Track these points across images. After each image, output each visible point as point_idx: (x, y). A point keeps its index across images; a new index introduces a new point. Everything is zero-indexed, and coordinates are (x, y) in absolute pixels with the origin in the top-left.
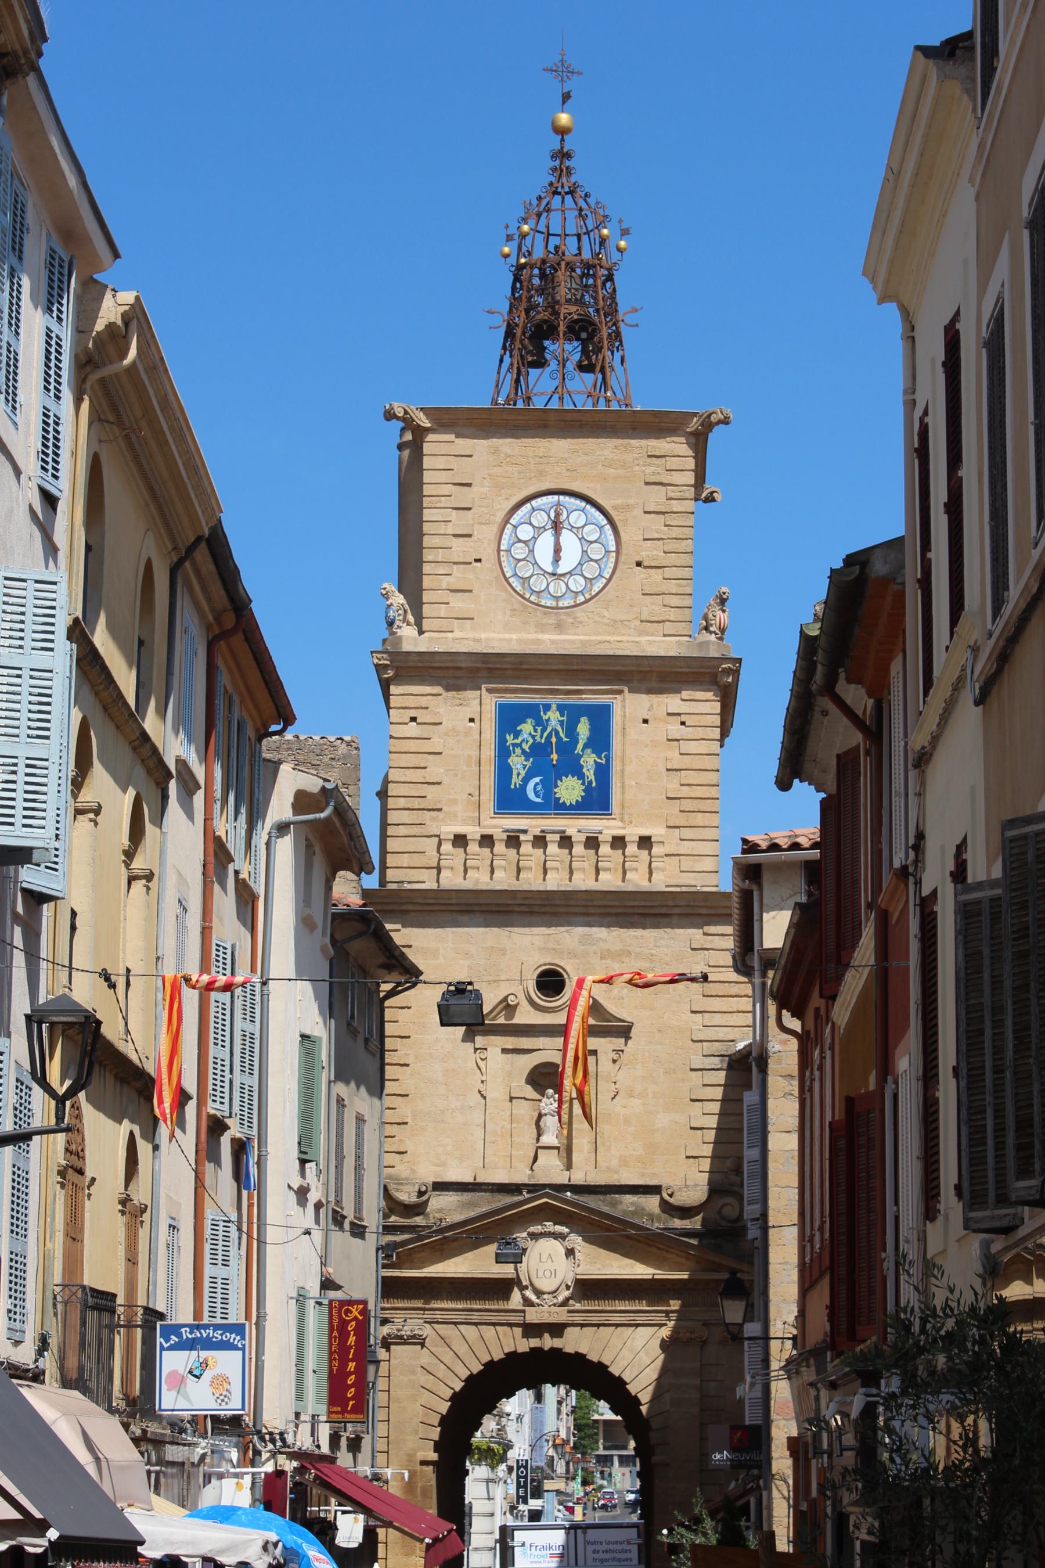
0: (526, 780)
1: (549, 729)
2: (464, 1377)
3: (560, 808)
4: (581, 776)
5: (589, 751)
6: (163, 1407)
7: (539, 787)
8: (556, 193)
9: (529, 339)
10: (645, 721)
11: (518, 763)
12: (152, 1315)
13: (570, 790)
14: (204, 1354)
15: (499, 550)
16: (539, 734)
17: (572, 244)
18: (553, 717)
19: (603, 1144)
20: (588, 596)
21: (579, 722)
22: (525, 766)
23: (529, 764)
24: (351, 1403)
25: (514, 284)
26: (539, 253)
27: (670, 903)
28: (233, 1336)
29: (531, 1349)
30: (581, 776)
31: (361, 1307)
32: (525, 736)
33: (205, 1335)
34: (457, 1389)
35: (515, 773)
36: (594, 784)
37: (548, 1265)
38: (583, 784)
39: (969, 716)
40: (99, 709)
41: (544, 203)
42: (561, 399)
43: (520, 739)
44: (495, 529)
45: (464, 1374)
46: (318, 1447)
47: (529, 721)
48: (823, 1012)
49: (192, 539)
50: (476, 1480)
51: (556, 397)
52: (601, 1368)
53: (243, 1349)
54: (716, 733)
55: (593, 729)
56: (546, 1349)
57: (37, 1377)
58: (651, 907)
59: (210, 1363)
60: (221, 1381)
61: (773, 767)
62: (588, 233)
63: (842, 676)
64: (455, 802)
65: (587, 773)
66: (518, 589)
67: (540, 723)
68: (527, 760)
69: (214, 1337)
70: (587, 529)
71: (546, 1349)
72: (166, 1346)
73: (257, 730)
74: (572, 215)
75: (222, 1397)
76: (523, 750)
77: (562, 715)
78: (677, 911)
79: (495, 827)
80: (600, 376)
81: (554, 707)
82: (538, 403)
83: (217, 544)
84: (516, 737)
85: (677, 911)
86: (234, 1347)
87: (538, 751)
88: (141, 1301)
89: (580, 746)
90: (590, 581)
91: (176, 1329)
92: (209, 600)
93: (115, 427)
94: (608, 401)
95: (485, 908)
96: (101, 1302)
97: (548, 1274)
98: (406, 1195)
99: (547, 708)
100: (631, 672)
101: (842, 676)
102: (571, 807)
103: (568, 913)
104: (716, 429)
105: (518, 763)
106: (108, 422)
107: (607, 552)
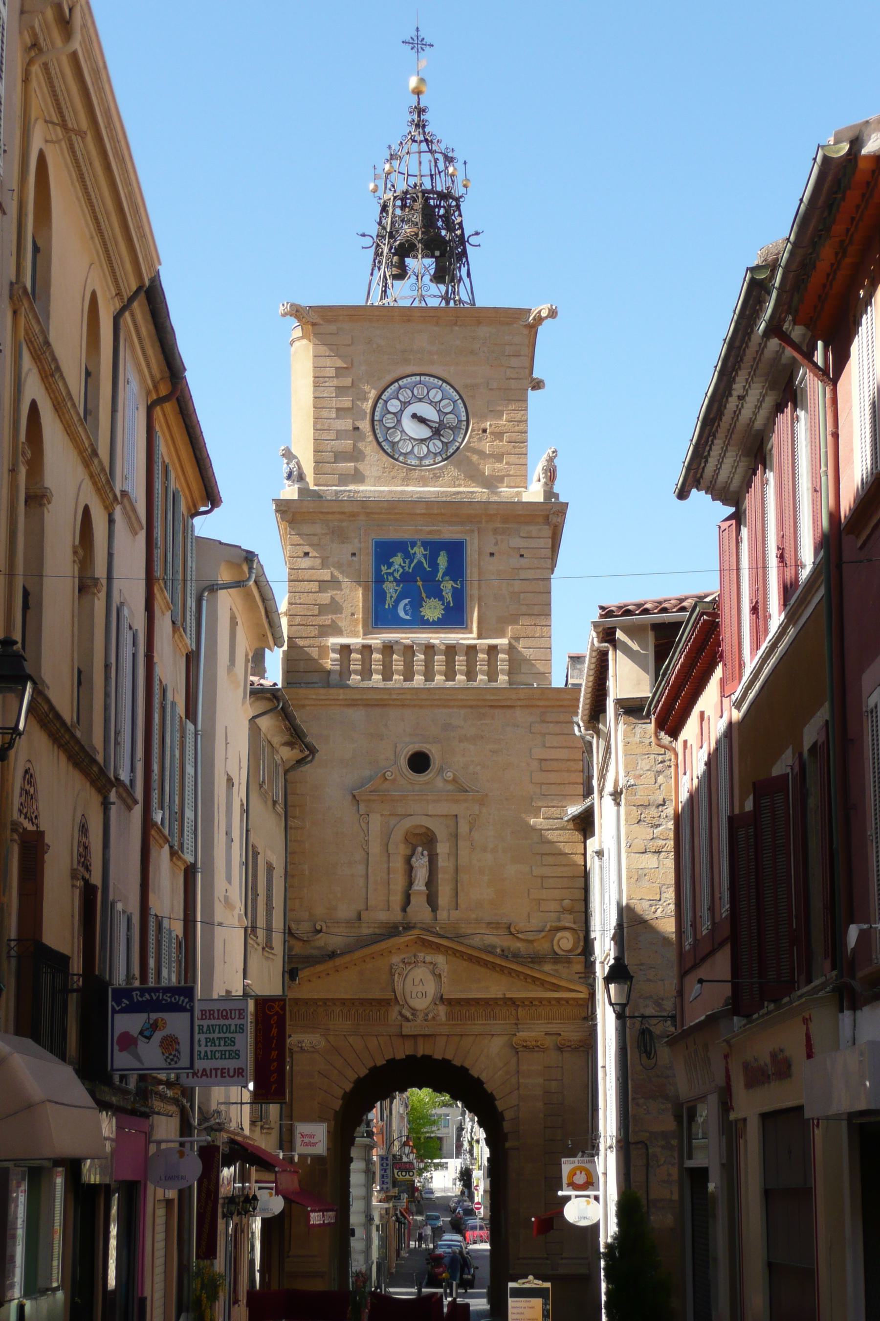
0: (397, 602)
1: (415, 561)
2: (369, 1067)
3: (424, 624)
4: (441, 598)
5: (447, 578)
6: (115, 1067)
7: (408, 608)
10: (492, 554)
11: (391, 589)
14: (154, 1016)
16: (407, 565)
18: (419, 552)
21: (439, 555)
22: (396, 590)
23: (399, 589)
24: (274, 1087)
25: (381, 213)
26: (402, 186)
27: (514, 697)
28: (182, 998)
29: (407, 1056)
30: (441, 598)
31: (282, 1003)
32: (397, 567)
33: (154, 998)
34: (348, 1090)
35: (388, 595)
36: (452, 605)
37: (420, 988)
38: (443, 604)
43: (392, 569)
45: (353, 1077)
46: (242, 1129)
47: (399, 554)
49: (134, 288)
51: (417, 299)
52: (463, 1071)
54: (548, 552)
55: (450, 561)
58: (498, 700)
59: (160, 1024)
60: (169, 1044)
62: (440, 173)
65: (446, 596)
66: (389, 451)
67: (408, 556)
68: (398, 585)
69: (163, 999)
70: (443, 403)
72: (117, 1009)
73: (189, 510)
75: (171, 1057)
76: (395, 578)
77: (425, 550)
78: (519, 703)
81: (419, 543)
83: (152, 298)
84: (389, 568)
85: (519, 703)
87: (406, 578)
89: (440, 574)
93: (58, 128)
97: (420, 995)
99: (413, 544)
102: (434, 623)
103: (431, 706)
104: (545, 323)
105: (391, 589)
107: (460, 421)
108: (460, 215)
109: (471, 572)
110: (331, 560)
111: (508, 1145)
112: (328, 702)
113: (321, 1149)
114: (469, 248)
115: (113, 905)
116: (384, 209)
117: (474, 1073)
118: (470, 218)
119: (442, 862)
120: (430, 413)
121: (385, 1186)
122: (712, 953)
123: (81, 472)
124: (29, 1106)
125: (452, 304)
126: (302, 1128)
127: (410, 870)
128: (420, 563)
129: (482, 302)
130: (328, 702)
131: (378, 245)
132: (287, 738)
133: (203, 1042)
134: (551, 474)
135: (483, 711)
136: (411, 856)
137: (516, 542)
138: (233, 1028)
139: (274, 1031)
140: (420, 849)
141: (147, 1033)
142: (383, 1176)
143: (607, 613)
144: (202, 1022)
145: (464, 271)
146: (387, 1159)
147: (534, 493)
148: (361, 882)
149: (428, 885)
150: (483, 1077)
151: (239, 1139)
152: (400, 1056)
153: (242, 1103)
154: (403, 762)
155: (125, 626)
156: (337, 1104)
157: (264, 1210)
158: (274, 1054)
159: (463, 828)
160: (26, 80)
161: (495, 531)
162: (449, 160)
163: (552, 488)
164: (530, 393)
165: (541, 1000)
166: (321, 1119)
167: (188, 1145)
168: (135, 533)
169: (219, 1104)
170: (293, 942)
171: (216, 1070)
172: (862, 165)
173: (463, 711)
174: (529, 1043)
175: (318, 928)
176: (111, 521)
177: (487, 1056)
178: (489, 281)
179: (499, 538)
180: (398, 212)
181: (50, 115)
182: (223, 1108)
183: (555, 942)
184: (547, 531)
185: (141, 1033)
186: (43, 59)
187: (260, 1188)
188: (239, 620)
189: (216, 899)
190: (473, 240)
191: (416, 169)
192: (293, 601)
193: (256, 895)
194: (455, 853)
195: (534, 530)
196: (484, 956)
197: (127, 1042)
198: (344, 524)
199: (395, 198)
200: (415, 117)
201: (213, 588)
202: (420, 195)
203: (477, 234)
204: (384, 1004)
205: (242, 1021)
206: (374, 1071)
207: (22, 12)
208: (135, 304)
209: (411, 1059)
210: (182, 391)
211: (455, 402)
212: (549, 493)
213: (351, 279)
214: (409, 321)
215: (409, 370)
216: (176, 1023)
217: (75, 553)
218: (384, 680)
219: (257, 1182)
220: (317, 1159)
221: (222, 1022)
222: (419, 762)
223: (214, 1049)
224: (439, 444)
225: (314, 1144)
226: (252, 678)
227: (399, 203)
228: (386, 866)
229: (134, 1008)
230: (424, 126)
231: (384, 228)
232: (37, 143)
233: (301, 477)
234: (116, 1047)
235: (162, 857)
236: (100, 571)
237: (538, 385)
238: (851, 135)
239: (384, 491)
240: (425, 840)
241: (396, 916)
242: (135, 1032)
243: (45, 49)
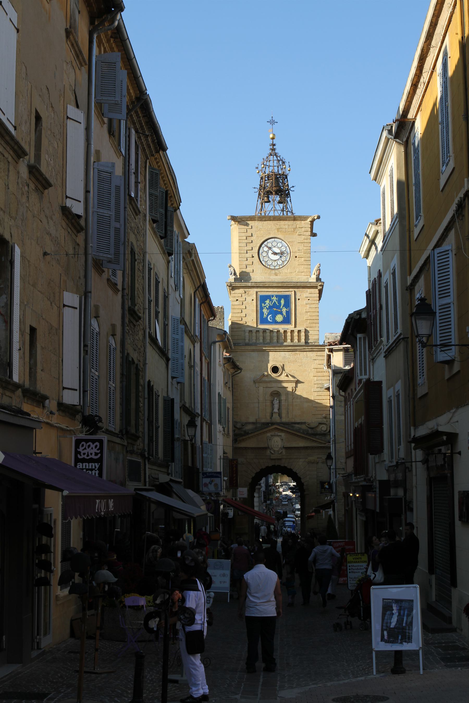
0: (268, 316)
3: (276, 322)
9: (265, 194)
11: (265, 311)
13: (279, 318)
14: (212, 479)
18: (274, 299)
48: (350, 394)
52: (291, 470)
53: (221, 478)
54: (318, 299)
60: (216, 485)
66: (264, 264)
87: (270, 307)
90: (283, 262)
98: (239, 426)
105: (265, 311)
108: (287, 180)
111: (305, 493)
113: (246, 496)
114: (290, 192)
116: (262, 178)
117: (294, 470)
118: (291, 181)
119: (283, 403)
120: (277, 251)
122: (350, 457)
127: (273, 405)
128: (275, 302)
132: (232, 367)
136: (273, 400)
139: (234, 469)
140: (276, 398)
141: (211, 483)
149: (278, 410)
150: (297, 472)
152: (270, 465)
156: (250, 481)
158: (234, 475)
162: (284, 163)
177: (299, 465)
190: (292, 189)
197: (206, 485)
200: (272, 147)
201: (215, 342)
203: (293, 187)
204: (266, 448)
206: (262, 470)
208: (200, 289)
209: (274, 466)
220: (244, 498)
229: (207, 477)
231: (262, 186)
235: (204, 423)
241: (268, 420)
242: (208, 482)
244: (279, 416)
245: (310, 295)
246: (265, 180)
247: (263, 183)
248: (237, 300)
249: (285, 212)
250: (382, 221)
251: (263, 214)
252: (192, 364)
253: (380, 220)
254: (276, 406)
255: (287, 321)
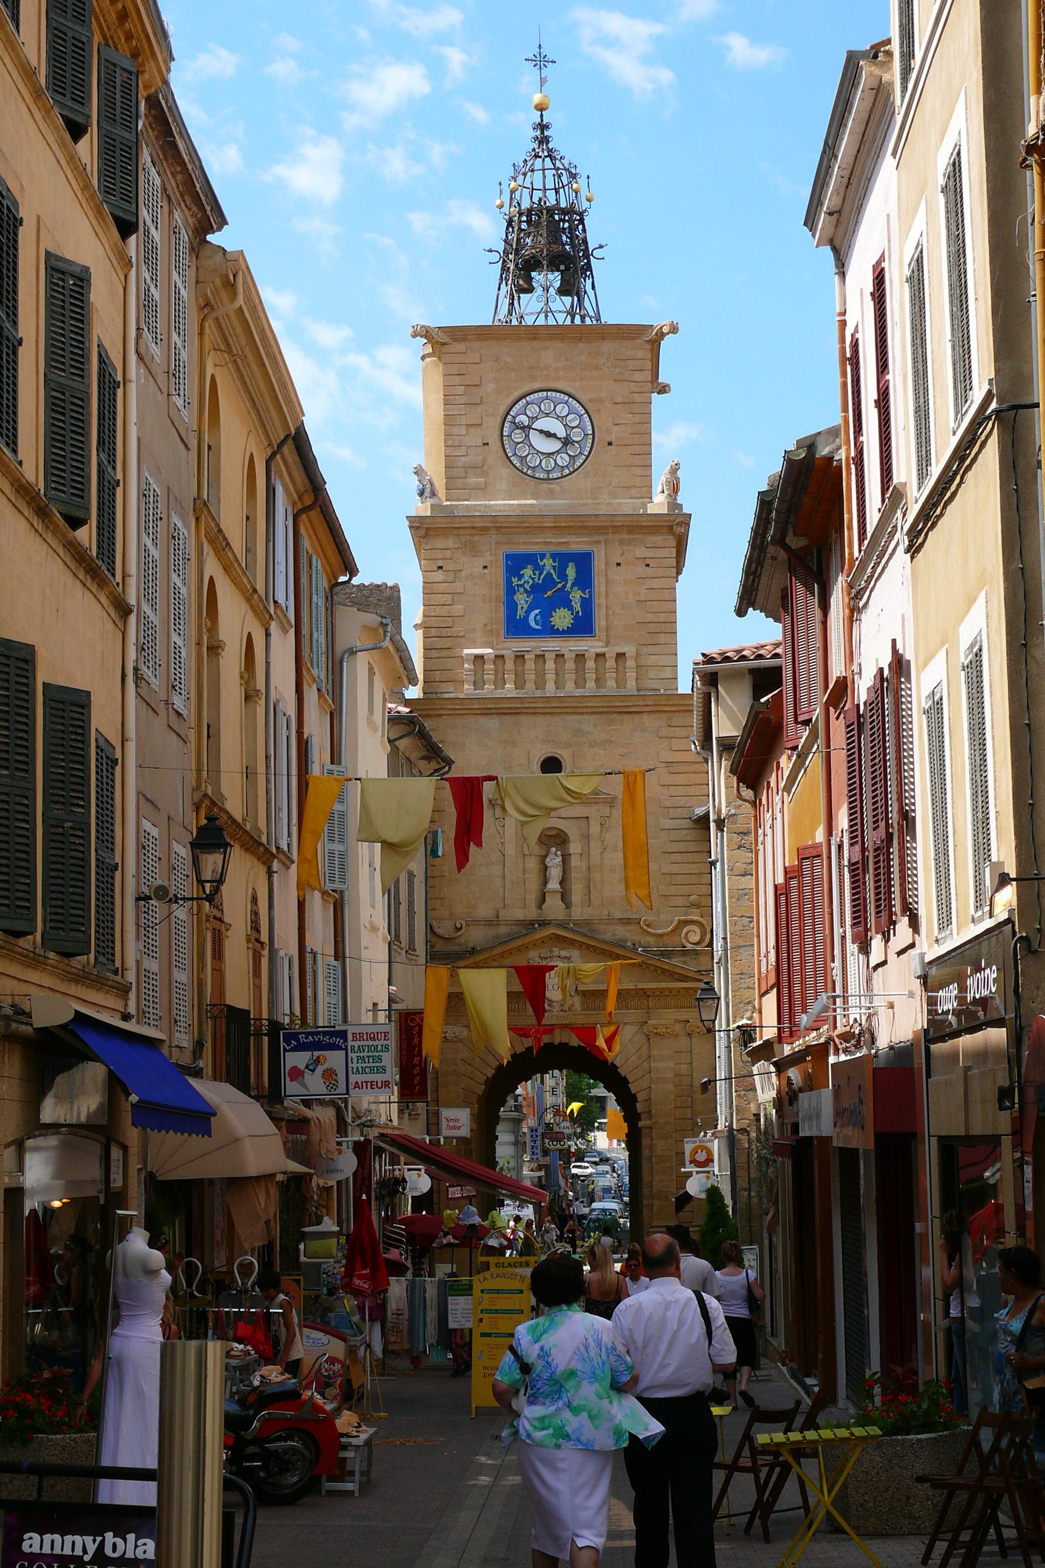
3: (553, 632)
4: (571, 608)
7: (538, 618)
8: (537, 156)
9: (520, 270)
10: (619, 564)
11: (522, 600)
12: (275, 1027)
13: (562, 618)
14: (316, 1053)
15: (502, 436)
16: (537, 577)
17: (551, 196)
18: (548, 563)
19: (595, 888)
20: (571, 469)
23: (529, 600)
25: (507, 229)
26: (526, 204)
30: (571, 608)
34: (490, 1075)
35: (519, 607)
39: (901, 558)
40: (220, 568)
41: (529, 164)
42: (546, 316)
44: (499, 420)
46: (391, 1121)
47: (529, 566)
50: (504, 1144)
51: (542, 315)
54: (674, 562)
56: (556, 1043)
57: (198, 1073)
59: (321, 1059)
60: (329, 1074)
61: (733, 600)
62: (563, 187)
63: (791, 531)
64: (474, 630)
70: (569, 418)
71: (556, 1043)
73: (330, 581)
74: (549, 174)
76: (525, 589)
78: (647, 709)
79: (506, 649)
80: (576, 298)
81: (548, 555)
82: (529, 321)
84: (520, 580)
85: (647, 709)
86: (340, 1048)
87: (536, 589)
88: (265, 1015)
89: (569, 585)
91: (295, 1036)
92: (294, 484)
94: (583, 318)
95: (500, 711)
96: (237, 1017)
99: (543, 556)
100: (606, 527)
101: (791, 531)
102: (564, 632)
105: (522, 600)
106: (221, 351)
107: (586, 435)
108: (584, 230)
109: (599, 583)
110: (463, 573)
111: (640, 1124)
112: (464, 712)
113: (465, 1132)
115: (277, 951)
116: (510, 223)
119: (574, 862)
121: (535, 1157)
123: (244, 607)
124: (237, 1140)
125: (578, 320)
126: (446, 1113)
128: (549, 574)
129: (607, 318)
130: (464, 712)
131: (504, 261)
132: (424, 753)
133: (355, 1060)
134: (674, 488)
135: (612, 717)
136: (546, 856)
137: (641, 552)
138: (380, 1048)
142: (533, 1147)
143: (708, 659)
144: (353, 1043)
145: (589, 282)
146: (536, 1130)
147: (658, 503)
148: (498, 882)
151: (389, 1131)
153: (390, 1103)
154: (536, 767)
155: (280, 715)
156: (480, 1089)
157: (413, 1189)
159: (595, 829)
160: (201, 334)
161: (621, 542)
162: (573, 176)
163: (675, 499)
164: (654, 395)
165: (670, 990)
166: (466, 1104)
167: (345, 1145)
168: (285, 631)
169: (369, 1103)
170: (434, 939)
171: (367, 1082)
172: (817, 462)
173: (593, 718)
174: (659, 1030)
175: (459, 926)
176: (268, 635)
178: (617, 295)
179: (626, 548)
180: (524, 226)
181: (218, 345)
182: (373, 1107)
183: (684, 931)
184: (672, 542)
185: (307, 1067)
186: (214, 315)
187: (409, 1170)
188: (376, 670)
189: (362, 927)
191: (541, 187)
192: (428, 613)
193: (398, 903)
194: (585, 854)
195: (659, 539)
196: (616, 950)
197: (296, 1074)
198: (476, 538)
199: (521, 214)
200: (538, 133)
201: (352, 652)
202: (545, 212)
203: (601, 247)
205: (386, 1042)
207: (197, 282)
208: (285, 449)
210: (324, 498)
211: (580, 416)
212: (674, 505)
213: (477, 297)
214: (535, 339)
215: (536, 386)
216: (334, 1059)
217: (242, 677)
218: (516, 689)
219: (405, 1164)
220: (462, 1140)
221: (370, 1043)
222: (552, 765)
223: (364, 1065)
224: (567, 458)
225: (459, 1128)
226: (390, 705)
227: (524, 218)
228: (522, 866)
229: (301, 1047)
230: (548, 142)
232: (210, 370)
233: (433, 494)
234: (288, 1079)
236: (261, 685)
237: (663, 389)
238: (808, 443)
239: (513, 505)
240: (556, 839)
241: (531, 913)
242: (302, 1067)
243: (215, 306)
244: (563, 899)
245: (648, 553)
246: (520, 230)
247: (515, 235)
248: (440, 568)
249: (578, 317)
250: (895, 47)
251: (515, 322)
252: (261, 685)
253: (888, 42)
254: (555, 873)
255: (583, 626)
